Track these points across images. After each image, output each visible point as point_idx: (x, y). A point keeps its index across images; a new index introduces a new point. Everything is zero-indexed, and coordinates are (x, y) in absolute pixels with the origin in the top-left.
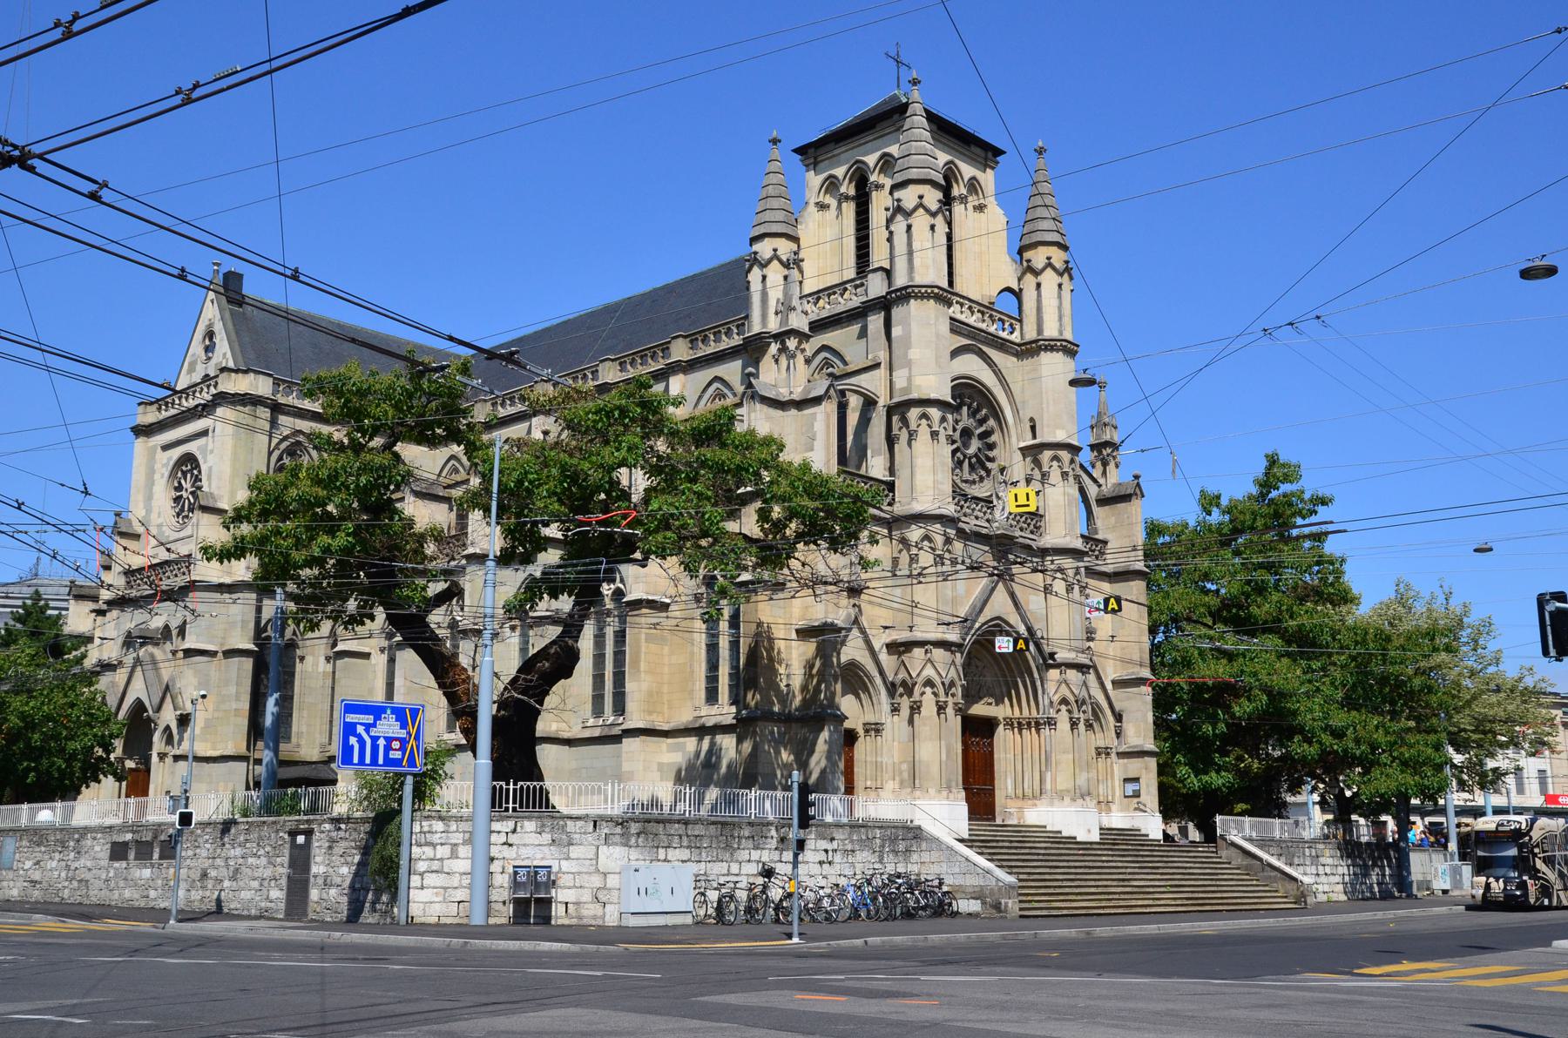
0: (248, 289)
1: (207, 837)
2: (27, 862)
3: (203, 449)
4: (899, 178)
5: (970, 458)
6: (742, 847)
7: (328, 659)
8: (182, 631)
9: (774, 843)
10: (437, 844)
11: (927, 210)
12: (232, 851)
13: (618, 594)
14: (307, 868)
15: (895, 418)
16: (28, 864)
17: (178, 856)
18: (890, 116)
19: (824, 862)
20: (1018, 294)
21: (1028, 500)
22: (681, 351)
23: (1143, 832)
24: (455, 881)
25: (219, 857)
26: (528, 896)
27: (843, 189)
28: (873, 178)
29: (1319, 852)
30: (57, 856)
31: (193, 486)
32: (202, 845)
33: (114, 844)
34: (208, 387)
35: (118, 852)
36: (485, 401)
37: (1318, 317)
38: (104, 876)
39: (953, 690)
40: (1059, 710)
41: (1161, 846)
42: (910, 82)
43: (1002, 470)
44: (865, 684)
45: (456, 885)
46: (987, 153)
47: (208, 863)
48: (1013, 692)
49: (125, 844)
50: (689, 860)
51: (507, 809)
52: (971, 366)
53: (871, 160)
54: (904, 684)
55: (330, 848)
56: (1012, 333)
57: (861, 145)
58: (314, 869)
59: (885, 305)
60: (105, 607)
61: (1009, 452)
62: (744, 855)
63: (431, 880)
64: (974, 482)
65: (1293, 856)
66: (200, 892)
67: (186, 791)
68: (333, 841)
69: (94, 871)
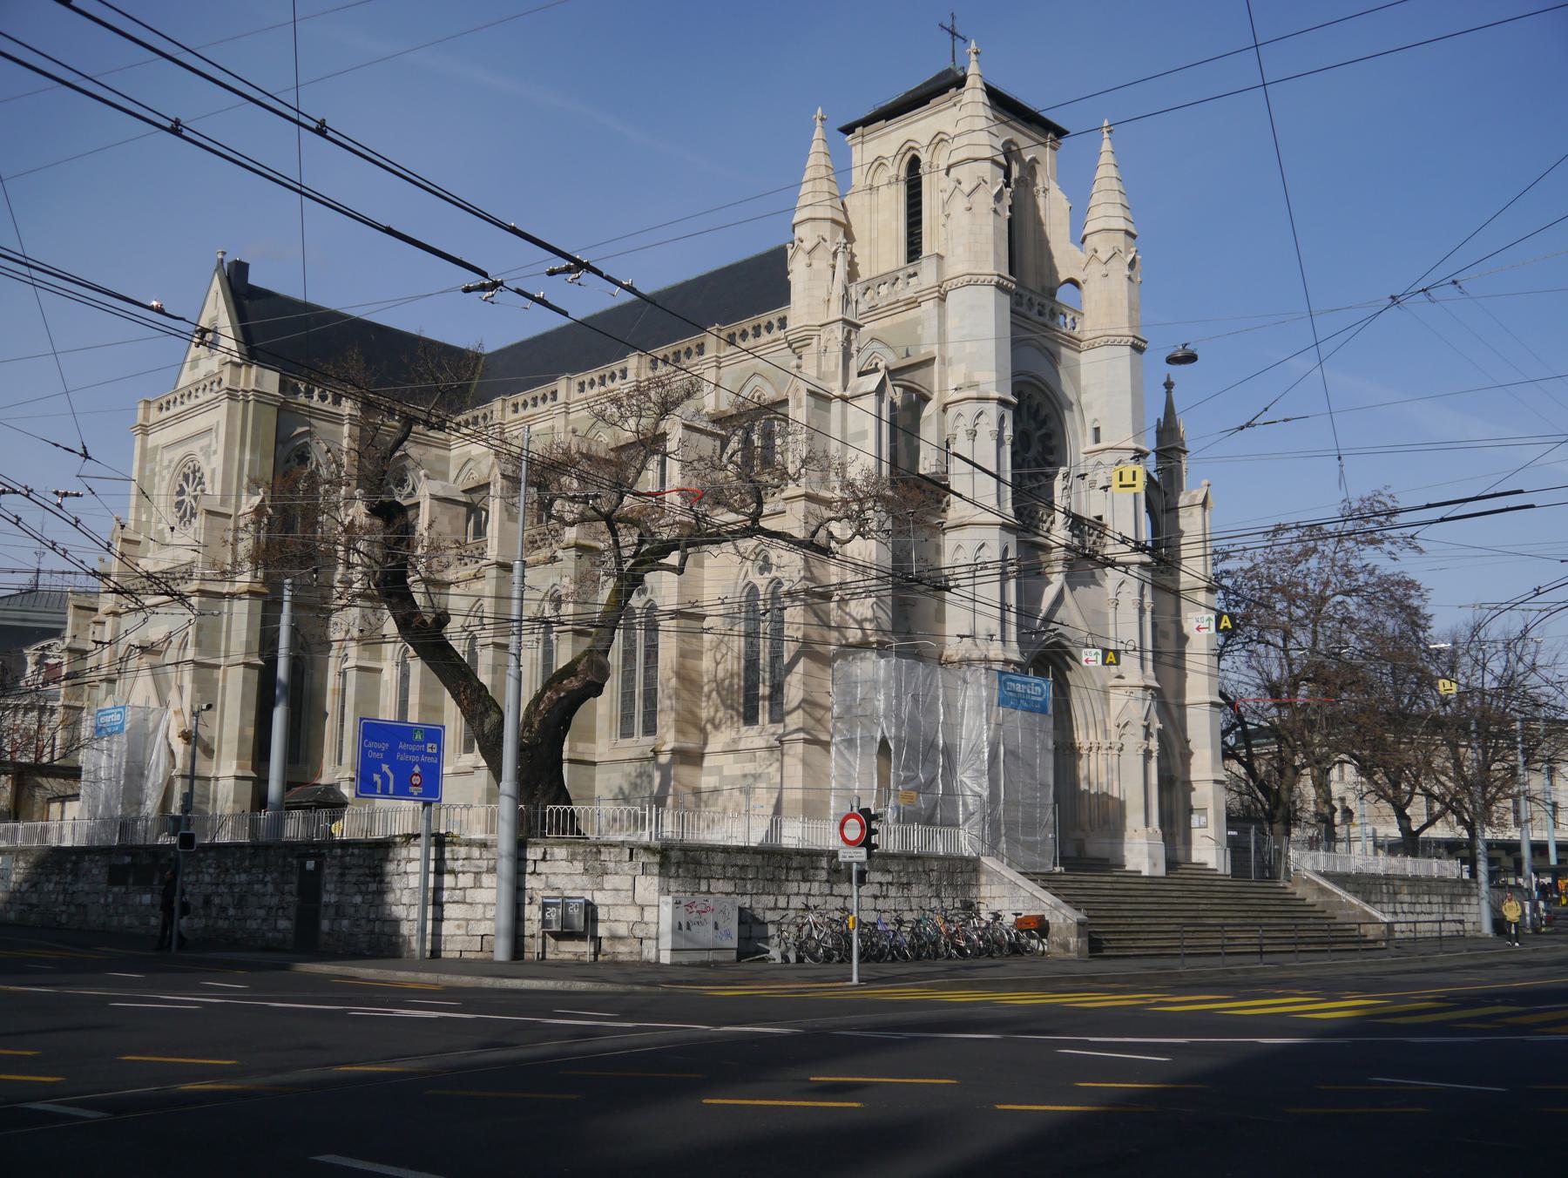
1: (210, 861)
9: (823, 875)
10: (459, 872)
12: (237, 877)
14: (318, 898)
21: (1134, 479)
25: (224, 883)
29: (1397, 889)
30: (55, 878)
32: (205, 870)
37: (1455, 282)
45: (479, 917)
46: (1053, 131)
55: (342, 875)
58: (326, 898)
62: (792, 887)
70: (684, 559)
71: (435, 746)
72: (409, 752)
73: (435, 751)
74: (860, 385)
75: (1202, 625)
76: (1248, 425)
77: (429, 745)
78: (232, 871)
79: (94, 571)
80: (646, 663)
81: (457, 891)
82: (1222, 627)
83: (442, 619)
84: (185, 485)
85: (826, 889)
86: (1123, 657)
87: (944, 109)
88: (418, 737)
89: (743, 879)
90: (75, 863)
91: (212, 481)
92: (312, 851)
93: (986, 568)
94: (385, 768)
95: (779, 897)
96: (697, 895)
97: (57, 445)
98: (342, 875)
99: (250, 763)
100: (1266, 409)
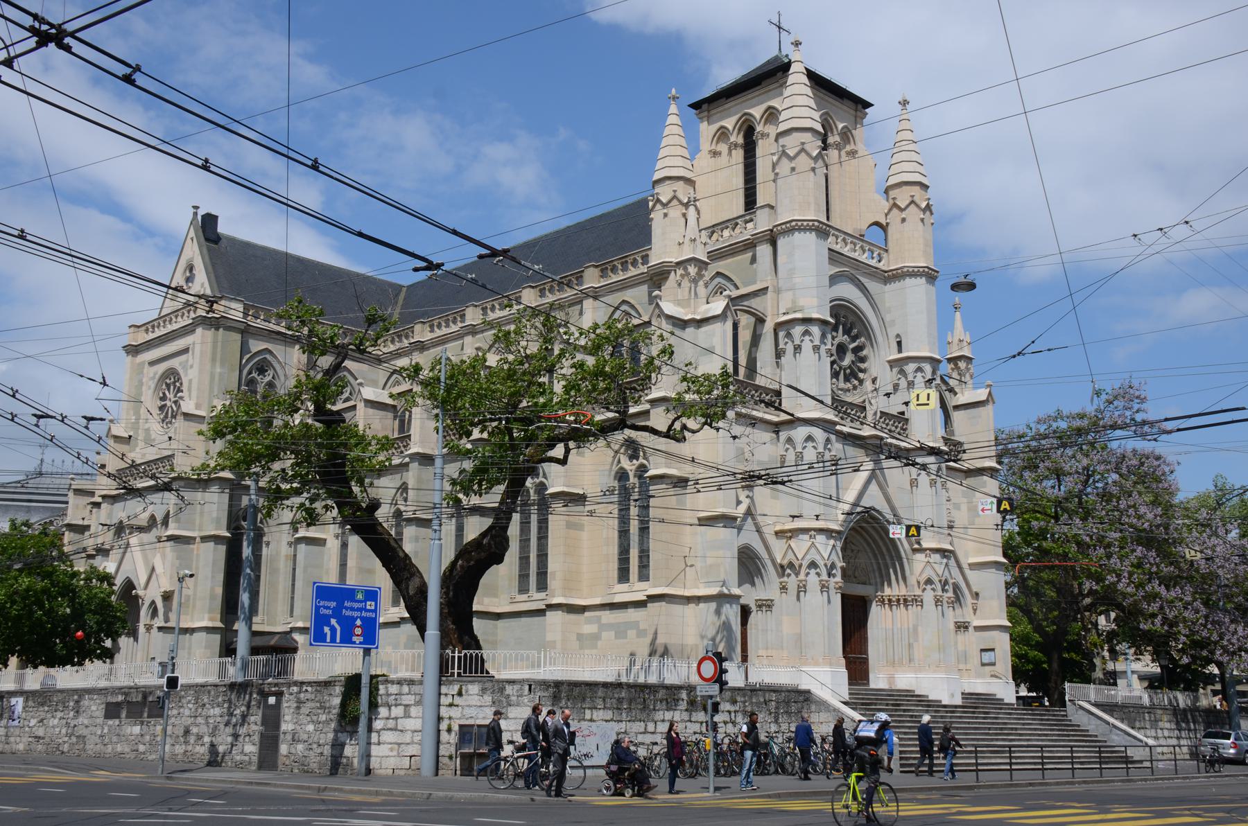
0: (222, 228)
1: (190, 698)
2: (32, 720)
3: (184, 365)
4: (782, 127)
5: (845, 370)
6: (657, 708)
7: (290, 544)
8: (165, 522)
9: (683, 705)
11: (681, 202)
12: (212, 710)
13: (541, 487)
14: (277, 726)
15: (781, 334)
16: (33, 722)
17: (165, 716)
18: (775, 72)
19: (728, 722)
20: (884, 228)
21: (928, 399)
22: (592, 279)
23: (998, 697)
24: (407, 737)
25: (200, 715)
26: (472, 751)
27: (733, 139)
28: (759, 128)
30: (59, 714)
31: (175, 396)
32: (185, 705)
33: (108, 705)
34: (189, 312)
35: (112, 711)
36: (476, 306)
37: (1187, 222)
38: (99, 732)
39: (834, 572)
40: (925, 589)
41: (1016, 709)
42: (792, 44)
43: (874, 381)
44: (760, 570)
45: (409, 741)
47: (190, 721)
48: (891, 571)
49: (118, 704)
50: (612, 720)
51: (453, 674)
52: (848, 291)
53: (757, 112)
54: (791, 565)
55: (298, 708)
56: (880, 261)
57: (747, 100)
58: (284, 727)
59: (772, 238)
60: (100, 500)
61: (878, 363)
62: (659, 715)
63: (388, 737)
64: (848, 390)
65: (1135, 720)
66: (184, 746)
67: (173, 658)
68: (299, 702)
69: (91, 728)
70: (567, 451)
71: (373, 603)
72: (352, 609)
73: (373, 608)
74: (708, 310)
75: (986, 507)
76: (1019, 354)
77: (368, 603)
78: (207, 705)
79: (109, 473)
80: (539, 533)
81: (391, 721)
82: (1002, 509)
83: (375, 505)
84: (167, 392)
85: (685, 716)
86: (922, 532)
87: (774, 89)
88: (360, 596)
89: (619, 709)
90: (77, 702)
91: (190, 390)
92: (273, 689)
93: (813, 467)
94: (333, 621)
95: (648, 724)
96: (583, 723)
97: (1049, 350)
98: (298, 708)
99: (219, 616)
100: (1033, 342)
